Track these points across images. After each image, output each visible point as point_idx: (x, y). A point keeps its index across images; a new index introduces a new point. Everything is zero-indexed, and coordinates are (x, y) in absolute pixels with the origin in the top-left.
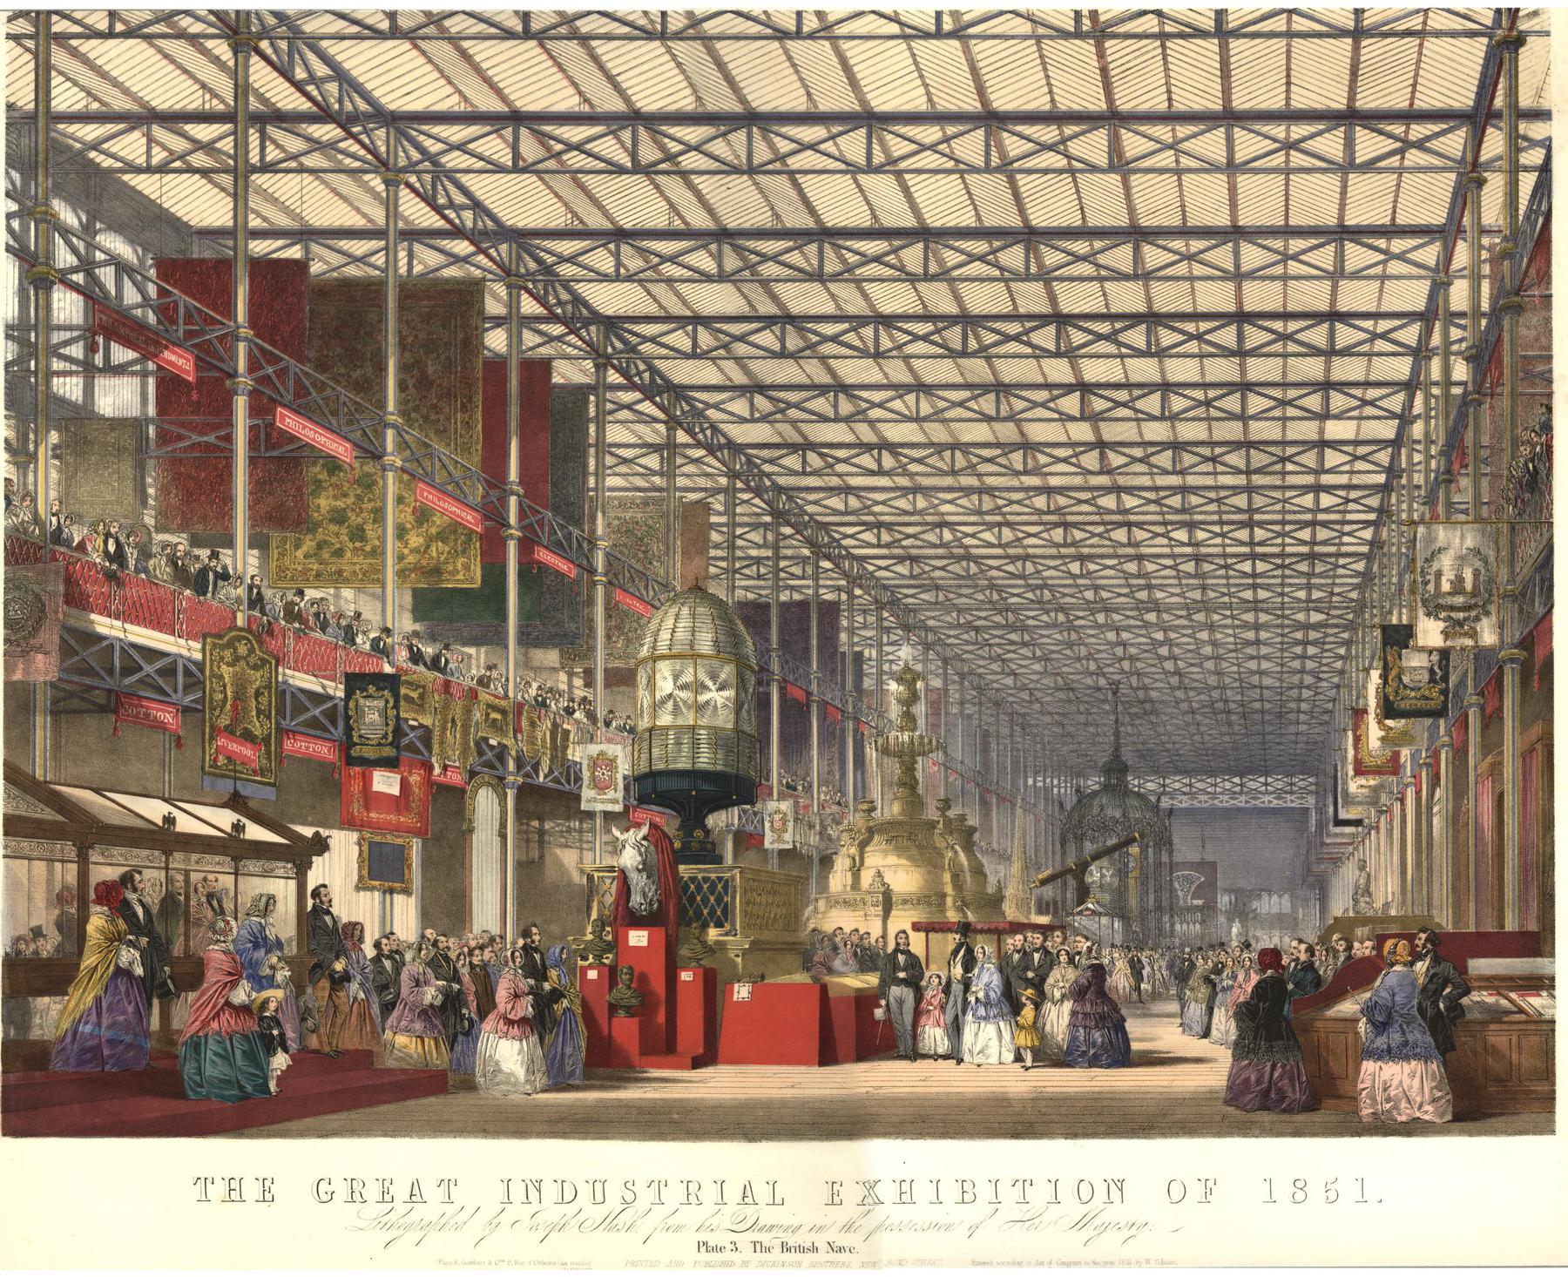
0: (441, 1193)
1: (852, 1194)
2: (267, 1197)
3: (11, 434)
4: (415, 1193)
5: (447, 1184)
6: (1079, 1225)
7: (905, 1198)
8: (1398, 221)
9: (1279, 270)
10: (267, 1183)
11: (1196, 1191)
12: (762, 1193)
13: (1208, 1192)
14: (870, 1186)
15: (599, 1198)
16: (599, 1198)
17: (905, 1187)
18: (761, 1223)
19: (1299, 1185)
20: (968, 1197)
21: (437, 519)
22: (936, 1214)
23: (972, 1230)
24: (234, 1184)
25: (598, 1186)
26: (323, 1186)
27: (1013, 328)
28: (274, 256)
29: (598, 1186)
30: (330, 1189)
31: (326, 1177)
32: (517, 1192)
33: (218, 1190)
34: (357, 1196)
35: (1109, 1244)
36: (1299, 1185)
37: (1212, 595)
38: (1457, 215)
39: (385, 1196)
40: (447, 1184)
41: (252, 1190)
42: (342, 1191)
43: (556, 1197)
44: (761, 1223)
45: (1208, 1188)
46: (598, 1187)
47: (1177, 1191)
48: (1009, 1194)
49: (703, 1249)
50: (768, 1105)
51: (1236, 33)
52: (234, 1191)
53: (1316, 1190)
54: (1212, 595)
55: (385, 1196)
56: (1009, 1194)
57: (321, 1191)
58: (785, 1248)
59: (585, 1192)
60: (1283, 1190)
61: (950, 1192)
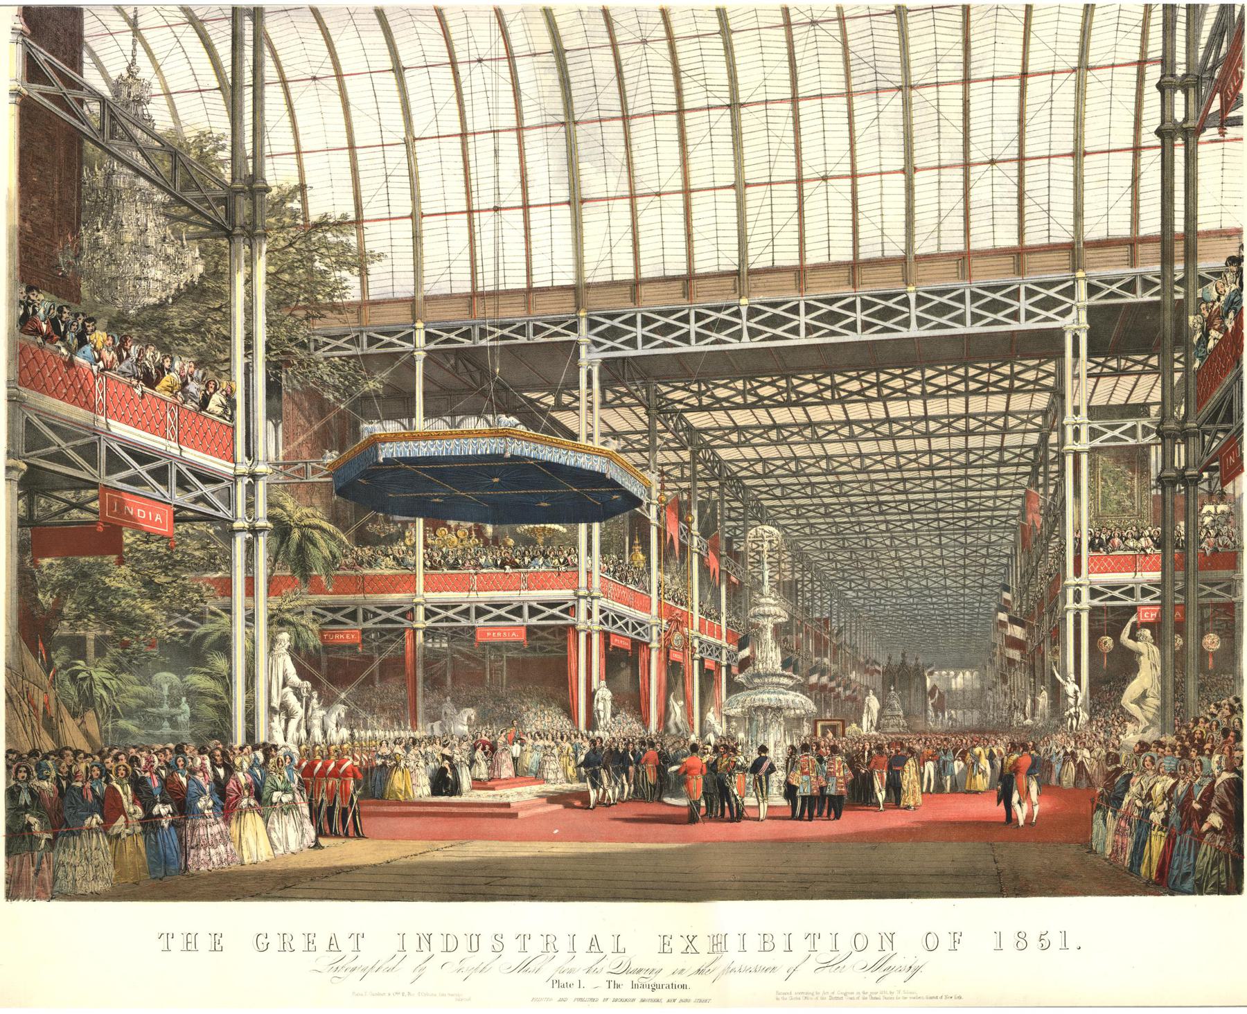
1: (702, 944)
2: (217, 947)
4: (332, 942)
5: (358, 937)
6: (876, 967)
7: (191, 946)
8: (886, 253)
9: (982, 429)
10: (311, 938)
11: (946, 942)
14: (691, 940)
15: (475, 947)
16: (475, 947)
18: (633, 967)
20: (768, 947)
22: (766, 960)
23: (792, 971)
25: (474, 939)
27: (844, 460)
29: (474, 939)
31: (264, 932)
32: (411, 943)
33: (177, 943)
34: (287, 947)
35: (894, 981)
36: (1021, 936)
37: (897, 542)
38: (1191, 527)
40: (358, 937)
41: (205, 942)
42: (276, 943)
43: (759, 946)
44: (633, 967)
45: (956, 938)
47: (932, 941)
48: (512, 945)
49: (556, 985)
52: (190, 943)
54: (897, 542)
55: (332, 942)
56: (512, 945)
57: (261, 943)
59: (464, 943)
60: (1009, 940)
61: (753, 943)
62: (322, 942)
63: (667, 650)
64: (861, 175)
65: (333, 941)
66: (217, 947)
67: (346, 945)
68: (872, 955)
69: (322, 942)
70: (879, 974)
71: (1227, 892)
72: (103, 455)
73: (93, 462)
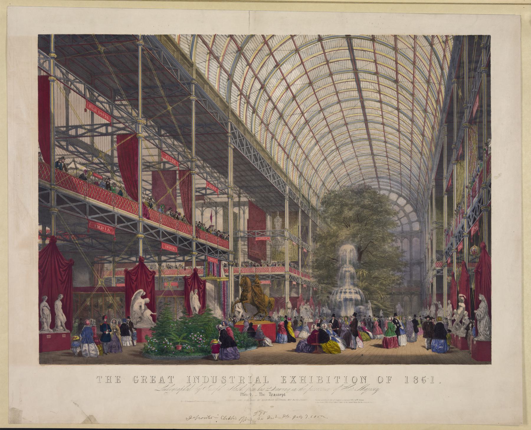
0: (169, 380)
2: (118, 381)
3: (40, 151)
4: (162, 380)
5: (171, 378)
10: (109, 378)
11: (386, 380)
12: (262, 380)
13: (389, 380)
16: (215, 381)
17: (109, 378)
19: (416, 379)
21: (454, 162)
24: (320, 378)
25: (215, 378)
26: (136, 378)
28: (449, 63)
29: (215, 378)
30: (137, 379)
33: (104, 379)
34: (242, 381)
39: (153, 381)
40: (171, 378)
42: (140, 380)
43: (151, 381)
44: (277, 388)
45: (389, 379)
46: (303, 379)
50: (376, 356)
51: (410, 221)
52: (144, 380)
53: (420, 380)
55: (162, 380)
58: (271, 395)
61: (315, 380)
62: (157, 380)
63: (73, 200)
64: (325, 64)
65: (162, 379)
66: (118, 381)
67: (167, 381)
68: (359, 385)
69: (157, 380)
70: (362, 391)
71: (56, 273)
72: (178, 240)
73: (159, 236)
